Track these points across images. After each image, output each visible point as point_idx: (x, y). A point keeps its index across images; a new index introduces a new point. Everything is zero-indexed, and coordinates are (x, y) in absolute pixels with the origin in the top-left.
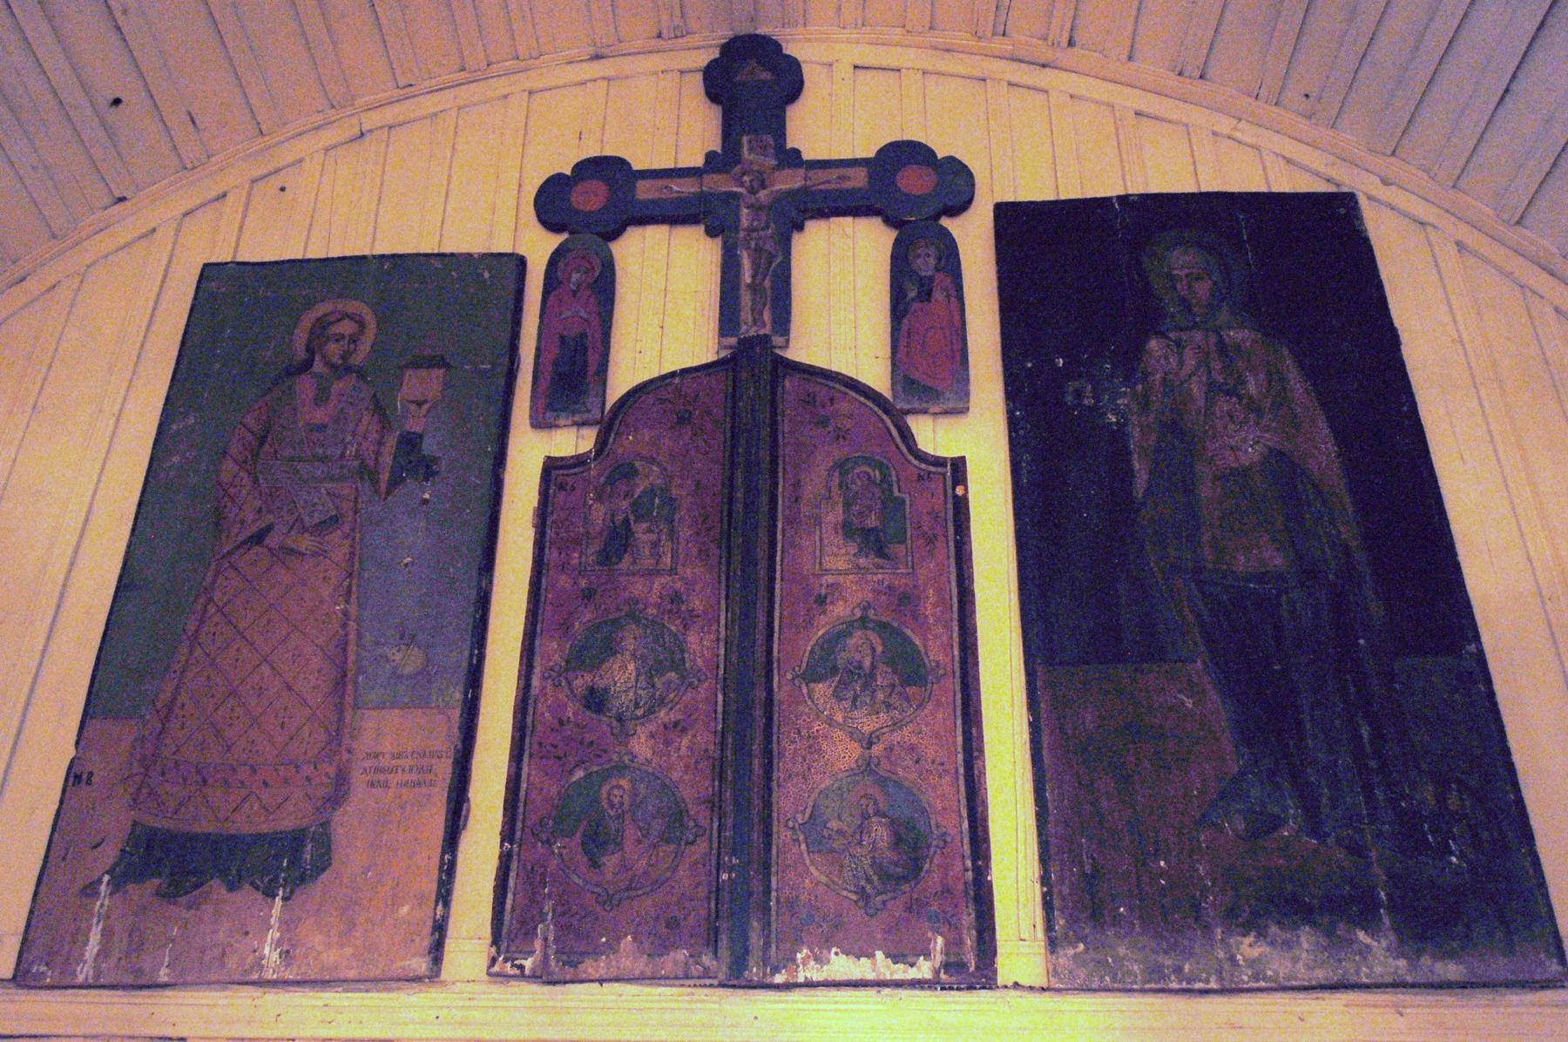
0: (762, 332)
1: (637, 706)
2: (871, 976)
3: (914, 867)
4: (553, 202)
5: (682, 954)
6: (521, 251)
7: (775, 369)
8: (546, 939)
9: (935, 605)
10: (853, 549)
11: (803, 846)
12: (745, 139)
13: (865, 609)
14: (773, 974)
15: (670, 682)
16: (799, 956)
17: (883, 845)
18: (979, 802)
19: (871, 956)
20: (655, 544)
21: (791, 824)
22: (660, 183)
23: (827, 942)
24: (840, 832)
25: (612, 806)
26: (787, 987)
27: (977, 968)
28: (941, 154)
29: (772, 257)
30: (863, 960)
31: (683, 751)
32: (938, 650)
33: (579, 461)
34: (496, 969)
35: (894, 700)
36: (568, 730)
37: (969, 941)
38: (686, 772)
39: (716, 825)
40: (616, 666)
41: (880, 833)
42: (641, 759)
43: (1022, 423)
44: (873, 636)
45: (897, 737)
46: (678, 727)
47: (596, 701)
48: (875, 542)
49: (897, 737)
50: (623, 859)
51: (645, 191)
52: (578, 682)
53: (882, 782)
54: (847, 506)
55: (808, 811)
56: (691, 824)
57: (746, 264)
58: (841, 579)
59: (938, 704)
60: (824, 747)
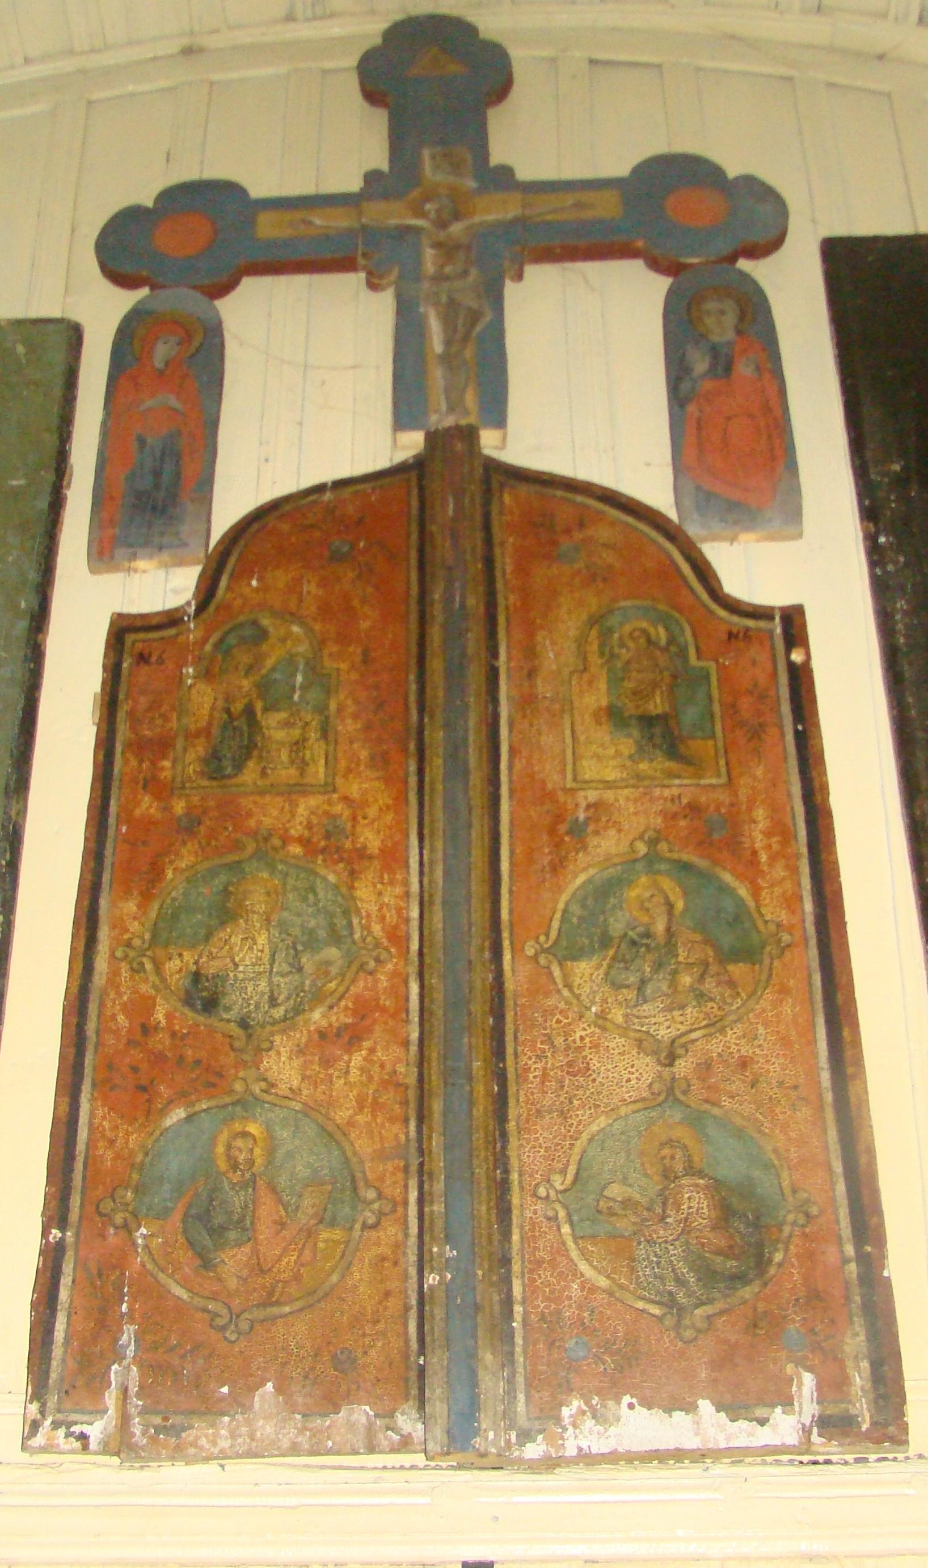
0: (463, 422)
1: (273, 1002)
2: (692, 1443)
3: (757, 1260)
4: (126, 248)
5: (361, 1413)
6: (75, 316)
7: (487, 480)
8: (125, 1390)
9: (768, 834)
10: (627, 746)
11: (566, 1229)
12: (426, 153)
13: (653, 842)
14: (521, 1444)
15: (328, 963)
16: (566, 1412)
17: (701, 1222)
18: (861, 1147)
19: (690, 1408)
20: (298, 745)
21: (542, 1191)
22: (298, 215)
23: (613, 1387)
24: (627, 1203)
25: (235, 1166)
26: (550, 1464)
27: (874, 1424)
28: (733, 171)
29: (475, 317)
30: (678, 1415)
31: (354, 1075)
32: (779, 903)
33: (172, 619)
34: (39, 1440)
35: (709, 985)
36: (160, 1041)
37: (859, 1379)
38: (361, 1108)
39: (413, 1195)
40: (236, 940)
41: (695, 1202)
42: (283, 1089)
43: (890, 553)
44: (667, 884)
45: (715, 1046)
46: (351, 1036)
47: (204, 995)
48: (662, 735)
49: (715, 1046)
50: (255, 1252)
51: (268, 227)
52: (174, 964)
53: (696, 1121)
54: (615, 681)
55: (572, 1170)
56: (371, 1194)
57: (435, 327)
58: (609, 795)
59: (784, 990)
60: (595, 1064)
